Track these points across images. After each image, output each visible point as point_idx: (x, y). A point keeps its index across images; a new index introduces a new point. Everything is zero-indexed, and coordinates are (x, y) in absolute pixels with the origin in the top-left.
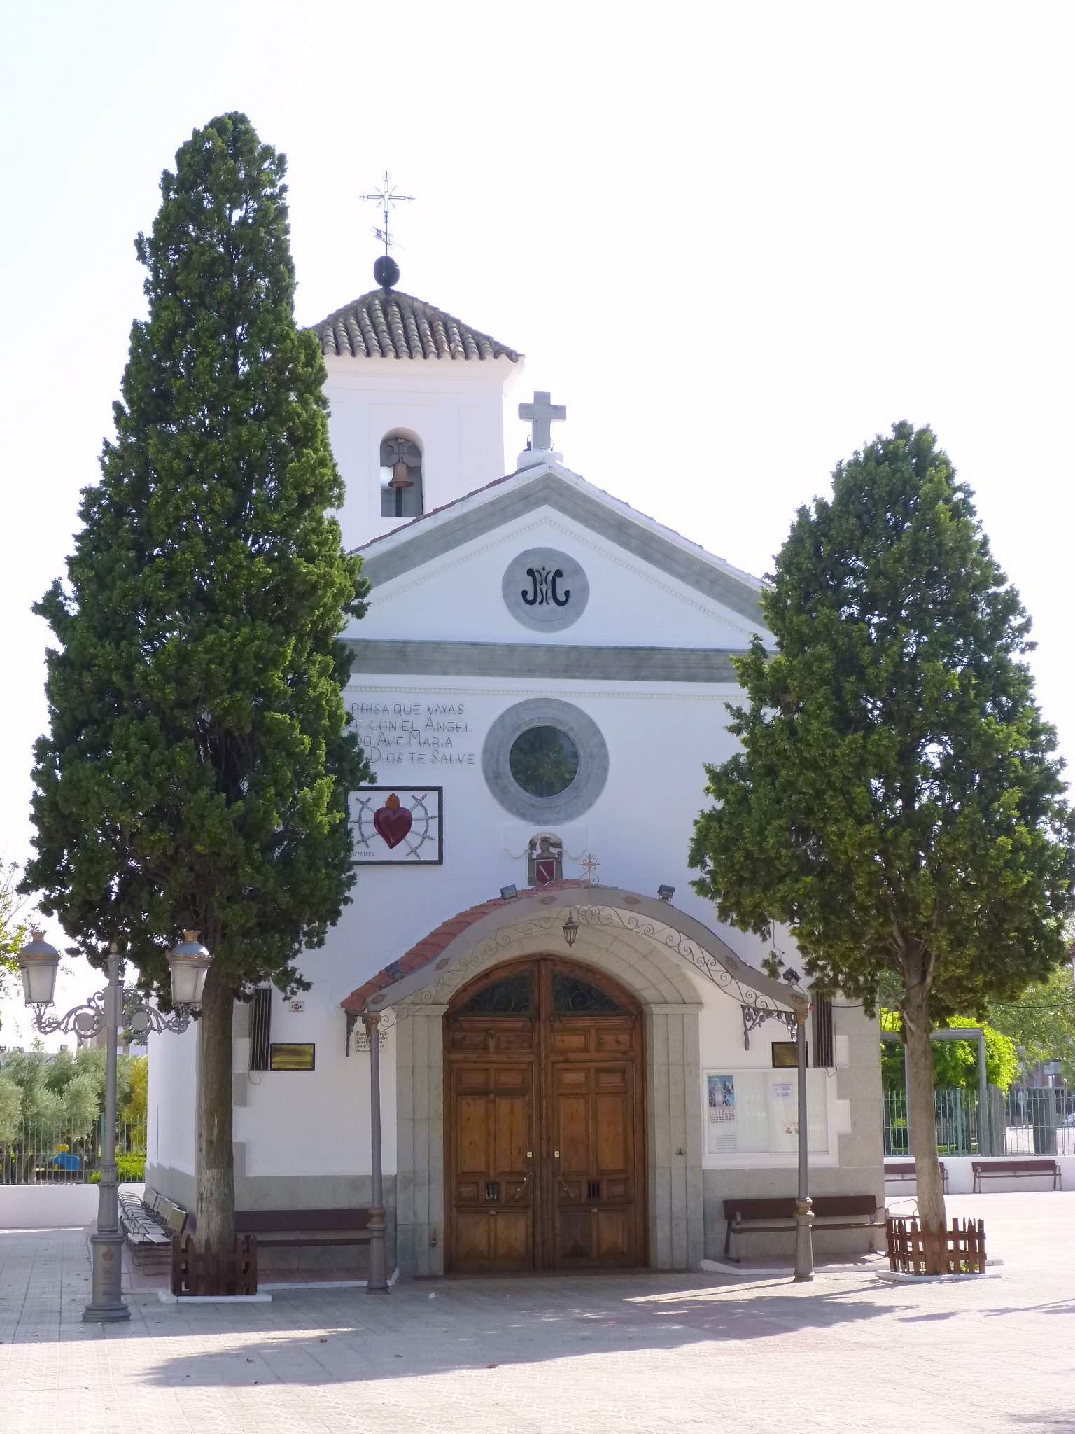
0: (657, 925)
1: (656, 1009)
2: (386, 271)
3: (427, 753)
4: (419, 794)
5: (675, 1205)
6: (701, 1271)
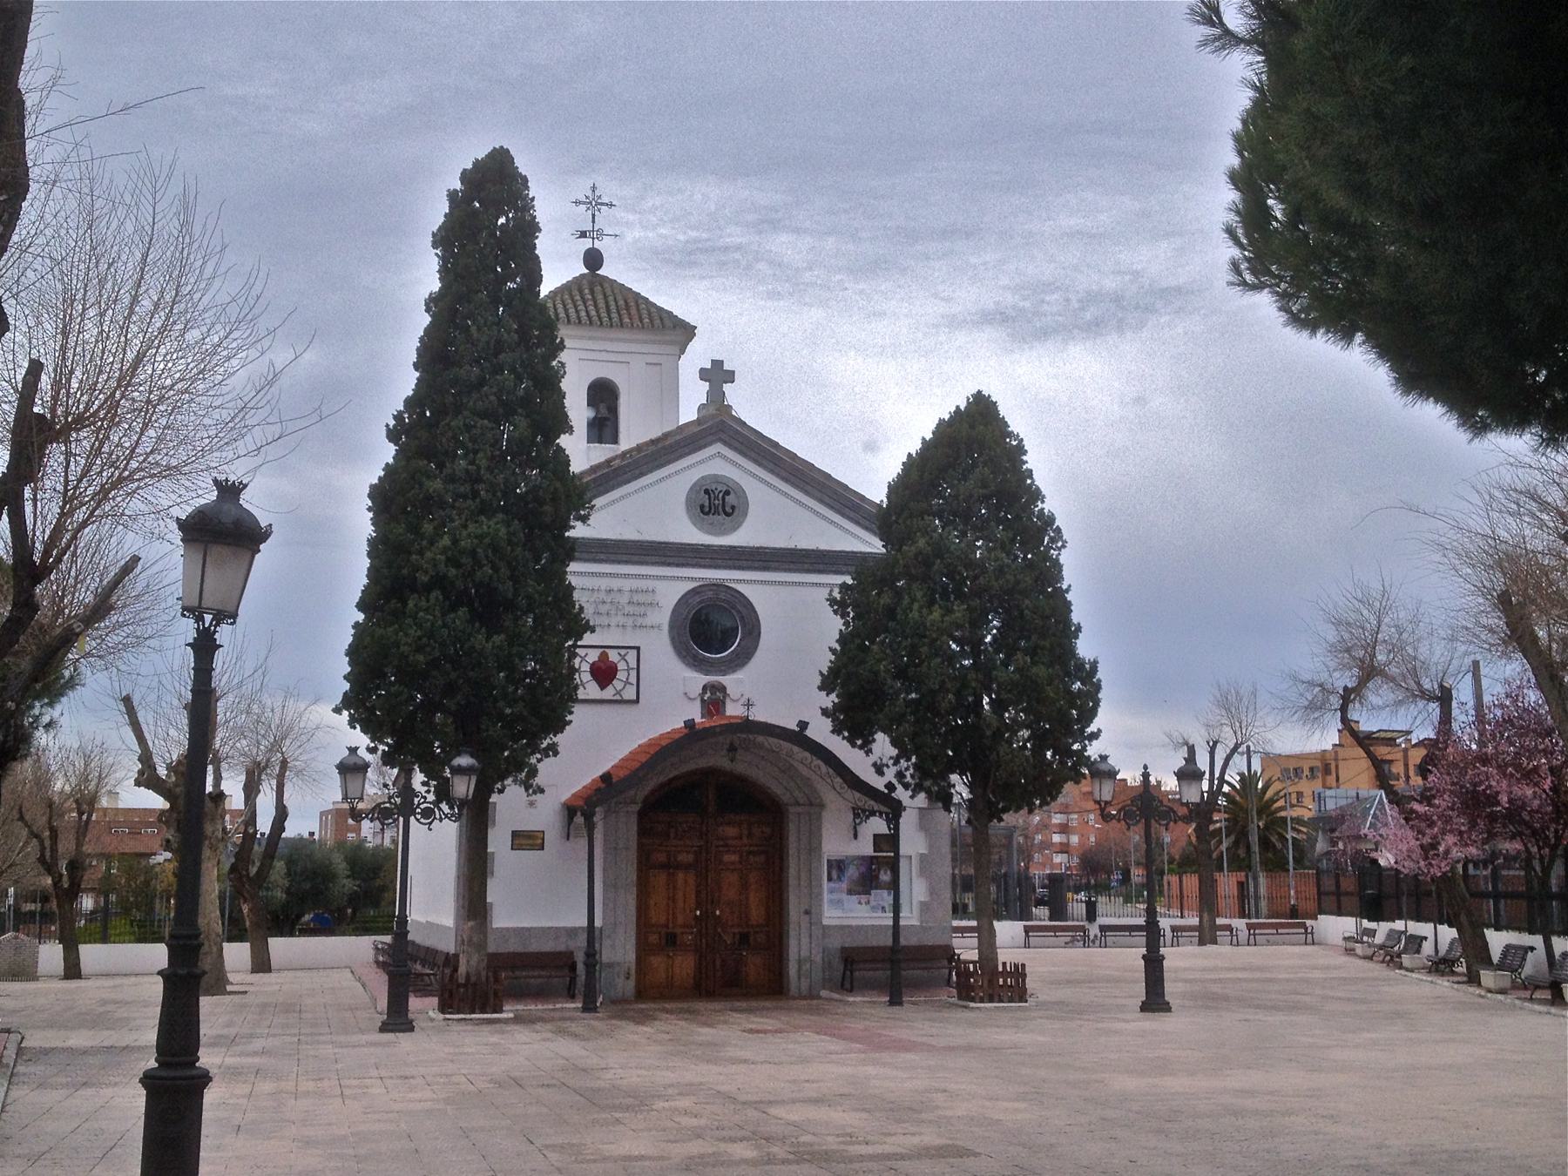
0: (796, 749)
1: (792, 809)
2: (593, 259)
3: (630, 622)
4: (623, 652)
5: (800, 947)
6: (819, 997)
